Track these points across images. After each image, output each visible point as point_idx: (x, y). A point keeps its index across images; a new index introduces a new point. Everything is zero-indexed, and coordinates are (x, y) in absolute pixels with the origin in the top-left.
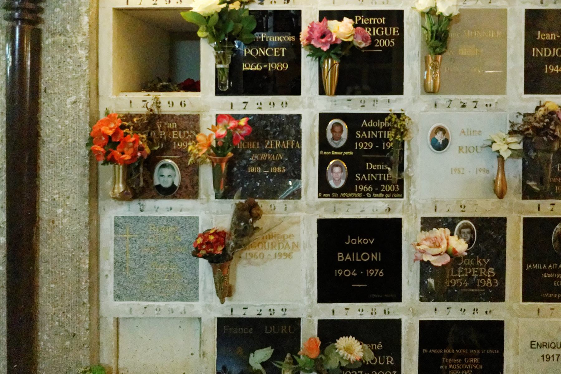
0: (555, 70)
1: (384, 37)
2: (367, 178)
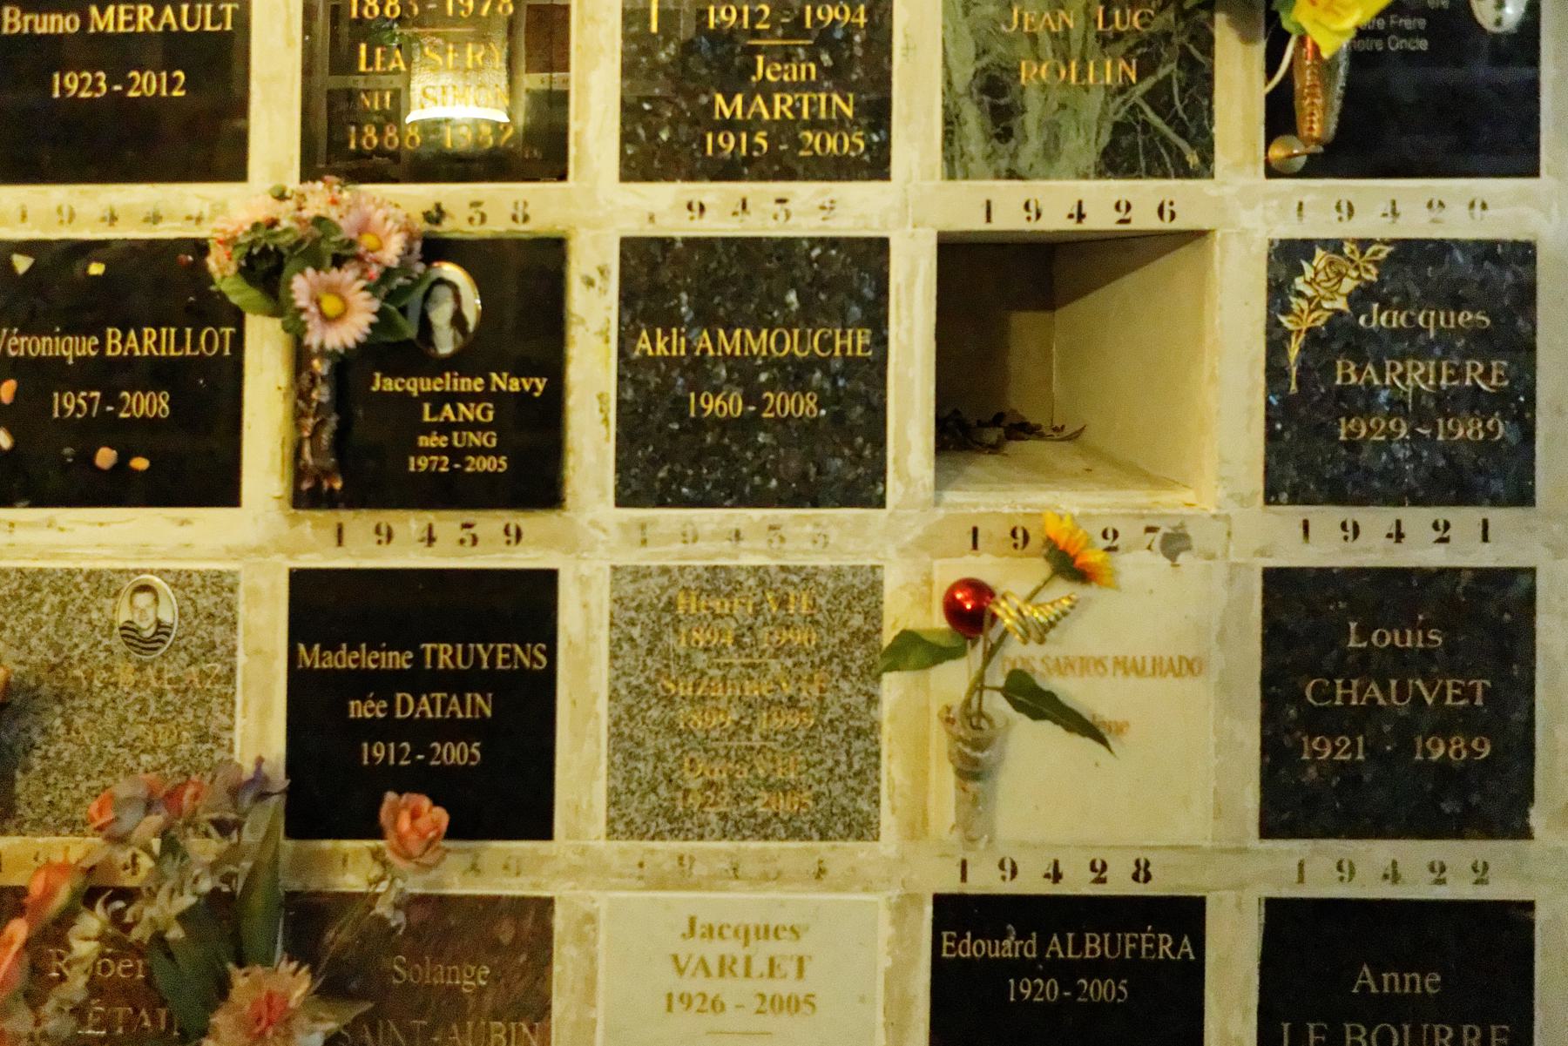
0: (853, 20)
1: (796, 87)
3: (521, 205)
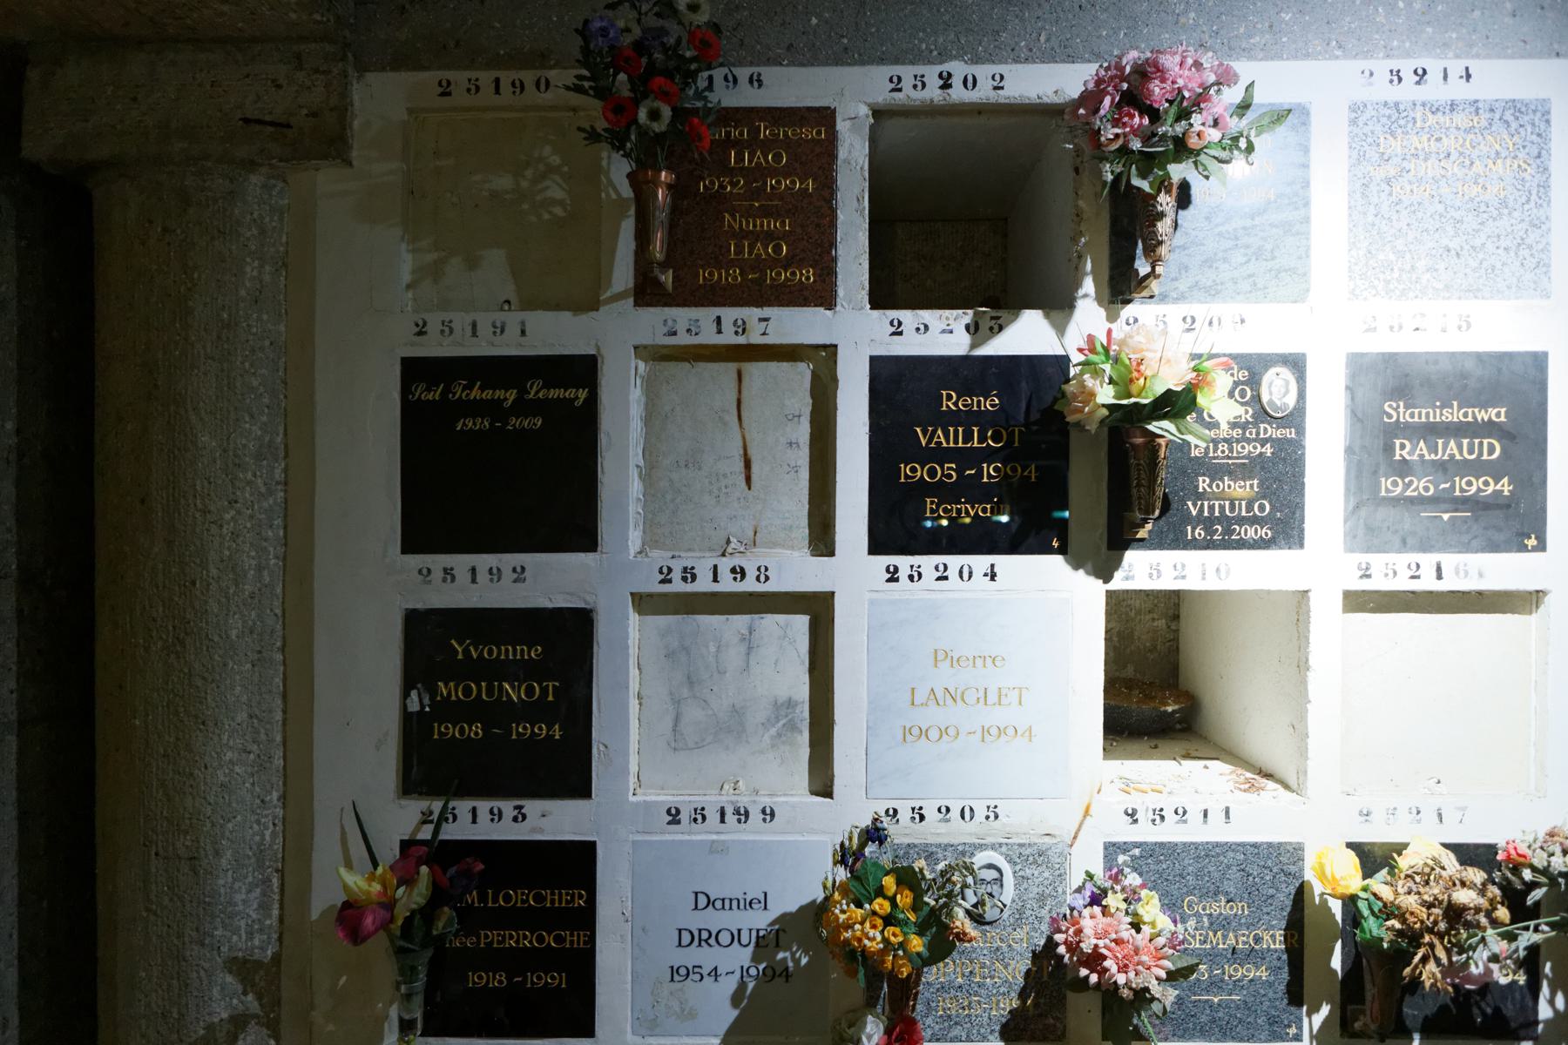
3: (763, 569)
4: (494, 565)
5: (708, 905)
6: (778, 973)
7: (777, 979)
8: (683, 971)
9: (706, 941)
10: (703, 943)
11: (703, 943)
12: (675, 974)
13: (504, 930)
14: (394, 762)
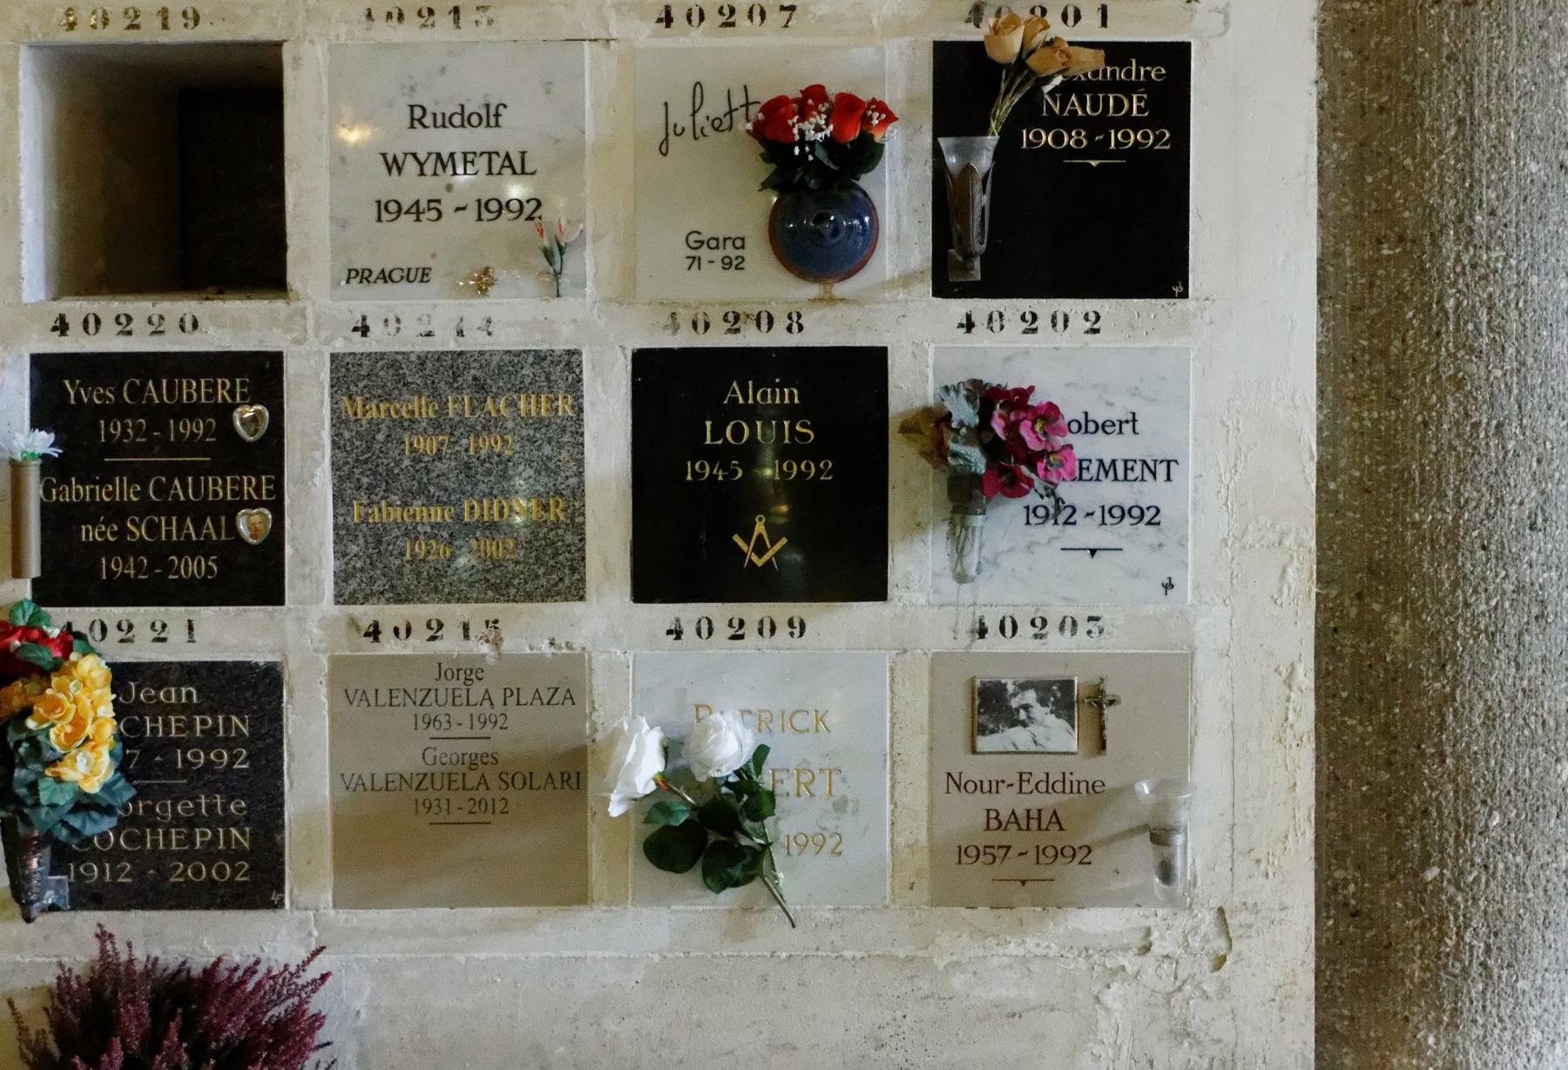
2: (746, 398)
3: (795, 317)
4: (1027, 310)
5: (1056, 856)
6: (404, 210)
7: (403, 216)
8: (494, 206)
9: (420, 121)
10: (416, 124)
11: (416, 124)
12: (483, 210)
13: (241, 475)
14: (180, 303)
